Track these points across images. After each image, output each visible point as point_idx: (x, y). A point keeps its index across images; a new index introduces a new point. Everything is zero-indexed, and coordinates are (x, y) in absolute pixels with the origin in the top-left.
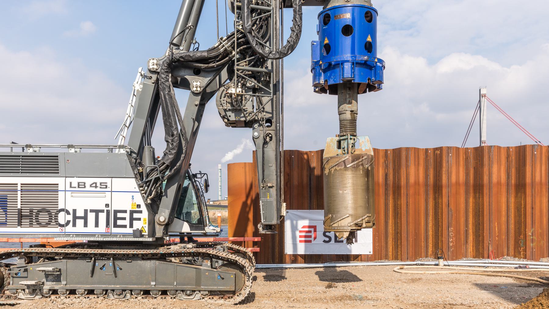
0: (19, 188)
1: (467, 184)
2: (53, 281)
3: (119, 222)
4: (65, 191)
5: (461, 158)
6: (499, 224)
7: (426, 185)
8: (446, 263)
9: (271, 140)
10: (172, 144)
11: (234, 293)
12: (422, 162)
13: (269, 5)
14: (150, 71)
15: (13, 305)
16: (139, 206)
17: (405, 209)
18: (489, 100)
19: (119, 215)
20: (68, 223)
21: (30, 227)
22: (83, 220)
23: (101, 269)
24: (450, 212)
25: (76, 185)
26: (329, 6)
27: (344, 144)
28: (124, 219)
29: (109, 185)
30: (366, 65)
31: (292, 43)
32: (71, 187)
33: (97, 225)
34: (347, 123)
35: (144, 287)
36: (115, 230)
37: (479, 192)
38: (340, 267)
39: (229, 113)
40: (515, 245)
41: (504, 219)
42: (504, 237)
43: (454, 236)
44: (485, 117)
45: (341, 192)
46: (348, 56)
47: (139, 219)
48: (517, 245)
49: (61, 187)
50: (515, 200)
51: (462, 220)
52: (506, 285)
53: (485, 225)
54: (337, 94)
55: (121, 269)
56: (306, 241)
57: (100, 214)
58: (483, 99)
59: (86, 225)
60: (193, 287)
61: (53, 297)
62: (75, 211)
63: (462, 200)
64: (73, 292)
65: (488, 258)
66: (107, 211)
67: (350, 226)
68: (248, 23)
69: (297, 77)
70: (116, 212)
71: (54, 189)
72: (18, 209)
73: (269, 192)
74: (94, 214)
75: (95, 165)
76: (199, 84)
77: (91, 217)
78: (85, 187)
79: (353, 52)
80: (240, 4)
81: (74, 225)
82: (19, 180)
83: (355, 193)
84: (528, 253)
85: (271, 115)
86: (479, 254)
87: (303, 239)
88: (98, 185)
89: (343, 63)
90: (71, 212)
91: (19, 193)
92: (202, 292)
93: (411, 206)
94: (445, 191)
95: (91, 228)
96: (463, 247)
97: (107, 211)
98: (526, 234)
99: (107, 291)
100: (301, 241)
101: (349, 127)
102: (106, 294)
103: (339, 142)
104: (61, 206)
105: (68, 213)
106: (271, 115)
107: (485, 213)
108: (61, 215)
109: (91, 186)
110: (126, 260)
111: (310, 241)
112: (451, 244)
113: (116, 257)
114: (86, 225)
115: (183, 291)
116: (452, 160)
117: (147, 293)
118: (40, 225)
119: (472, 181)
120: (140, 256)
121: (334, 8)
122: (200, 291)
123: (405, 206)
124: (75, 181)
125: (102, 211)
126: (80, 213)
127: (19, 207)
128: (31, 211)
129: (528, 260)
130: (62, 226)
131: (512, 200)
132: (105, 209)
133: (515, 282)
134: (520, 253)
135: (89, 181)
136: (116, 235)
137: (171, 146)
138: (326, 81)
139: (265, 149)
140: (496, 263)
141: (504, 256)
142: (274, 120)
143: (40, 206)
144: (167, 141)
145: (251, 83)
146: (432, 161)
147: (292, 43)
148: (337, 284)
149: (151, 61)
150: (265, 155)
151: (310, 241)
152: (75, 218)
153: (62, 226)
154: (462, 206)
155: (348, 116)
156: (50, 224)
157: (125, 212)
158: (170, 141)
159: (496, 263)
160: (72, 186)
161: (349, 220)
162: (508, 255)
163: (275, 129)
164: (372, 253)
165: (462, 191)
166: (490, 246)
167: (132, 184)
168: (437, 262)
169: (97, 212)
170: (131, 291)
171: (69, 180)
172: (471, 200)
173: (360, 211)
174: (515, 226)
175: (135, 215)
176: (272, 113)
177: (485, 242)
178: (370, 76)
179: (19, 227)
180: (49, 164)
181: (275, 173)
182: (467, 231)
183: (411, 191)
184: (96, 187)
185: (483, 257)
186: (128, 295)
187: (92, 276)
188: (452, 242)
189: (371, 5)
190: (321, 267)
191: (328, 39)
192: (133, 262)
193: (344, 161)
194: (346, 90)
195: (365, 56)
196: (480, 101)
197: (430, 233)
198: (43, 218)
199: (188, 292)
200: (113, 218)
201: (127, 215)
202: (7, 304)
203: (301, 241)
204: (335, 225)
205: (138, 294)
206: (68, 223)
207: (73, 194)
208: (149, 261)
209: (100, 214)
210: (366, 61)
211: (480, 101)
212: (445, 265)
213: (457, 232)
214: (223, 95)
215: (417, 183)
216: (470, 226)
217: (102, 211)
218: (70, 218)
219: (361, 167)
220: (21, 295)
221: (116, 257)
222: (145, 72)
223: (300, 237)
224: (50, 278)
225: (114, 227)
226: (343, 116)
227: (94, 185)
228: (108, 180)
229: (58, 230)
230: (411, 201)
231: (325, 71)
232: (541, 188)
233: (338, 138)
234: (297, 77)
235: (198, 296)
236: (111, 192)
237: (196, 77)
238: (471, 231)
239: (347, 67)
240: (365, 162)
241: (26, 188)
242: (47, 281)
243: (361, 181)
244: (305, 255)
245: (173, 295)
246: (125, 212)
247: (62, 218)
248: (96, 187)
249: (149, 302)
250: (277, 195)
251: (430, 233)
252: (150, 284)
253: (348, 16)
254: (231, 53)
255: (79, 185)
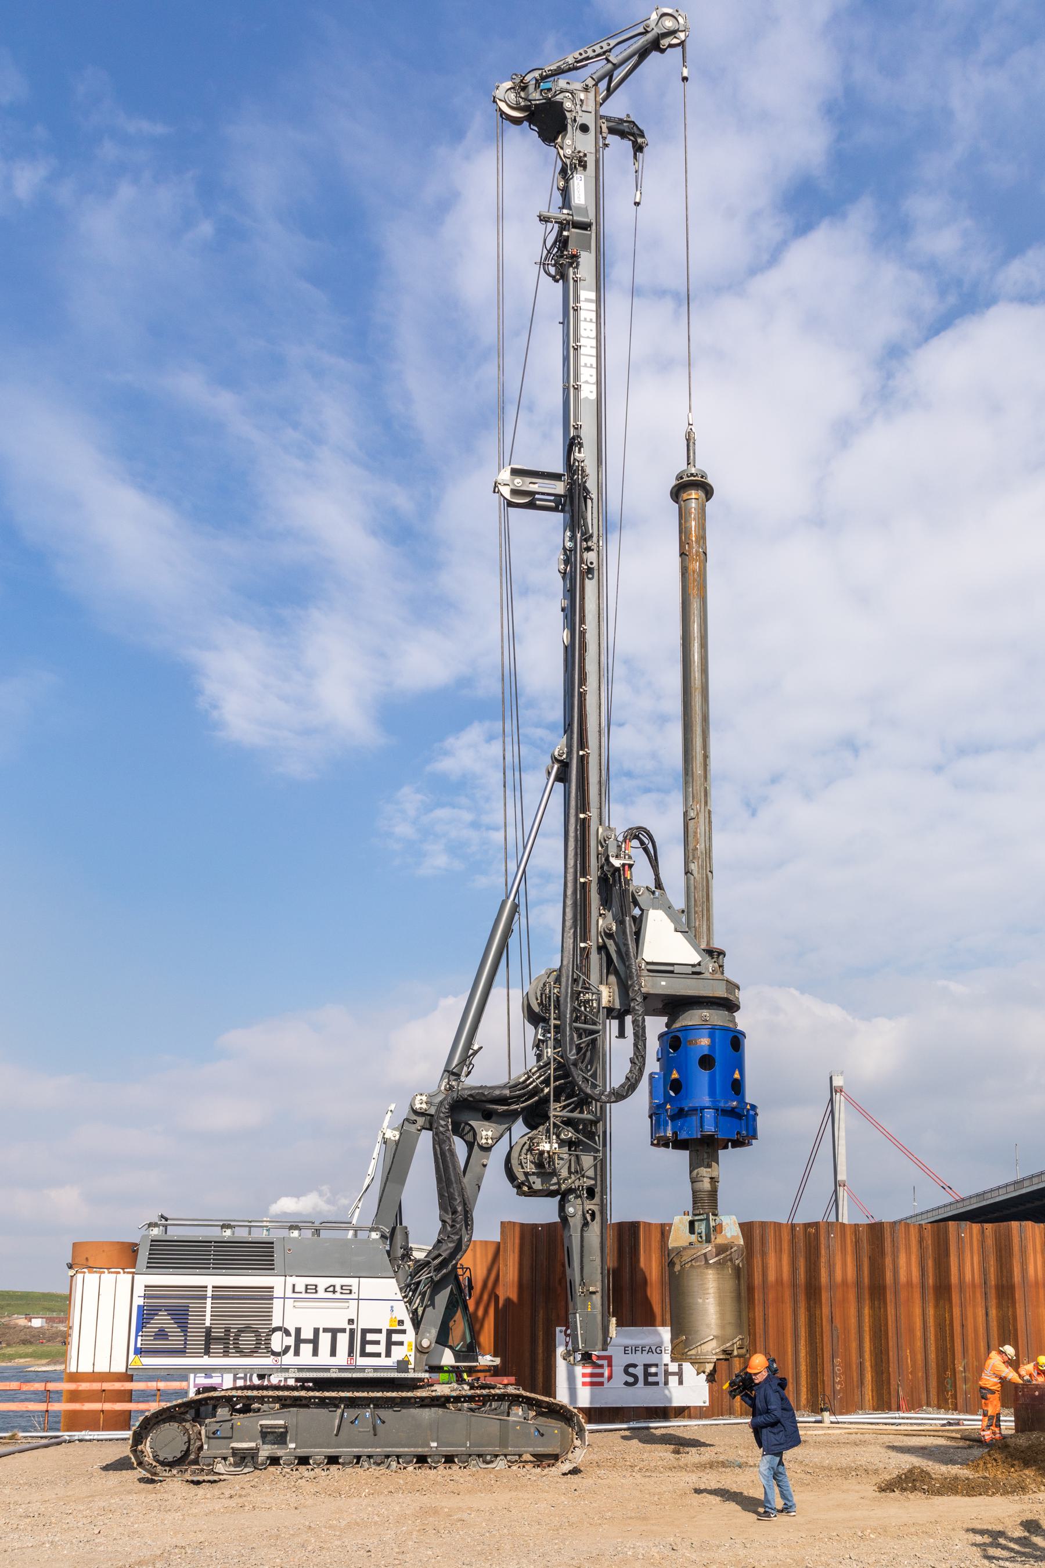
0: (209, 1293)
1: (858, 1284)
2: (274, 1444)
3: (369, 1349)
4: (284, 1298)
5: (849, 1241)
6: (913, 1353)
7: (794, 1285)
8: (833, 1418)
9: (593, 1219)
10: (452, 1226)
11: (556, 1457)
12: (786, 1246)
13: (594, 1023)
14: (415, 1112)
15: (215, 1481)
16: (401, 1322)
17: (762, 1326)
18: (849, 1100)
19: (370, 1337)
20: (287, 1349)
21: (224, 1356)
22: (311, 1345)
23: (352, 1422)
24: (835, 1333)
25: (303, 1290)
26: (677, 1025)
27: (700, 1227)
28: (378, 1343)
29: (355, 1289)
30: (733, 1113)
31: (633, 1081)
32: (294, 1292)
33: (333, 1353)
34: (703, 1195)
35: (420, 1450)
36: (362, 1361)
37: (879, 1299)
38: (656, 1428)
39: (532, 1179)
40: (938, 1387)
41: (919, 1344)
42: (920, 1374)
43: (842, 1374)
44: (843, 1134)
45: (700, 1301)
46: (706, 1100)
47: (401, 1343)
48: (941, 1389)
49: (278, 1292)
50: (935, 1312)
51: (854, 1345)
52: (938, 1447)
53: (891, 1354)
54: (687, 1149)
55: (384, 1422)
56: (592, 1384)
57: (339, 1335)
58: (837, 1097)
59: (315, 1353)
60: (497, 1450)
61: (271, 1469)
62: (298, 1331)
63: (853, 1311)
64: (304, 1461)
65: (899, 1409)
66: (351, 1330)
67: (716, 1354)
68: (571, 1050)
69: (629, 1121)
70: (365, 1332)
71: (266, 1295)
72: (206, 1328)
73: (591, 1300)
74: (329, 1335)
75: (327, 1254)
76: (490, 1133)
77: (325, 1339)
78: (316, 1292)
79: (712, 1093)
80: (558, 1022)
81: (297, 1353)
82: (210, 1281)
83: (721, 1303)
84: (960, 1401)
85: (593, 1182)
86: (883, 1403)
87: (588, 1380)
88: (338, 1288)
89: (702, 1109)
90: (293, 1333)
91: (209, 1301)
92: (509, 1458)
93: (771, 1322)
94: (825, 1296)
95: (324, 1358)
96: (857, 1392)
97: (351, 1330)
98: (954, 1369)
99: (358, 1458)
100: (584, 1384)
101: (705, 1203)
102: (358, 1463)
103: (692, 1224)
104: (276, 1322)
105: (287, 1333)
106: (593, 1182)
107: (890, 1334)
108: (277, 1337)
109: (326, 1291)
110: (392, 1407)
111: (601, 1384)
112: (838, 1387)
113: (378, 1403)
114: (315, 1353)
115: (479, 1456)
116: (836, 1245)
117: (422, 1459)
118: (241, 1353)
119: (866, 1280)
120: (413, 1401)
121: (686, 1029)
122: (505, 1456)
123: (762, 1321)
124: (301, 1283)
125: (343, 1331)
126: (307, 1334)
127: (208, 1324)
128: (227, 1331)
129: (960, 1412)
130: (274, 1354)
131: (931, 1311)
132: (348, 1327)
133: (949, 1443)
134: (946, 1400)
135: (323, 1283)
136: (362, 1369)
137: (449, 1229)
138: (675, 1133)
139: (585, 1234)
140: (911, 1418)
141: (922, 1406)
142: (598, 1190)
143: (242, 1323)
144: (443, 1221)
145: (568, 1134)
146: (801, 1245)
147: (633, 1081)
148: (687, 1449)
149: (419, 1097)
150: (585, 1244)
151: (601, 1384)
152: (299, 1341)
153: (274, 1354)
154: (853, 1321)
155: (706, 1185)
156: (256, 1352)
157: (379, 1331)
158: (449, 1221)
159: (911, 1418)
160: (296, 1290)
161: (713, 1344)
162: (928, 1405)
163: (599, 1202)
164: (707, 1404)
165: (852, 1296)
166: (900, 1389)
167: (390, 1287)
168: (819, 1418)
169: (334, 1332)
170: (398, 1457)
171: (291, 1280)
172: (866, 1311)
173: (730, 1330)
174: (937, 1356)
175: (395, 1337)
176: (595, 1179)
177: (893, 1382)
178: (739, 1125)
179: (206, 1357)
180: (259, 1255)
181: (599, 1271)
182: (861, 1364)
183: (771, 1296)
184: (334, 1292)
185: (890, 1409)
186: (394, 1464)
187: (106, 1468)
188: (839, 1382)
189: (736, 1024)
190: (625, 1430)
191: (678, 1072)
192: (404, 1411)
193: (705, 1255)
194: (704, 1149)
195: (733, 1101)
196: (831, 1100)
197: (803, 1368)
198: (247, 1340)
199: (488, 1458)
200: (360, 1340)
201: (382, 1337)
202: (204, 1481)
203: (584, 1384)
204: (693, 1352)
205: (409, 1463)
206: (287, 1349)
207: (296, 1304)
208: (427, 1410)
209: (339, 1335)
210: (733, 1109)
211: (831, 1100)
212: (832, 1423)
213: (847, 1366)
214: (524, 1151)
215: (779, 1282)
216: (867, 1356)
217: (343, 1331)
218: (290, 1341)
219: (729, 1263)
220: (220, 1468)
221: (378, 1403)
222: (405, 1113)
223: (584, 1375)
224: (270, 1438)
225: (361, 1356)
226: (698, 1185)
227: (331, 1289)
228: (353, 1282)
229: (269, 1361)
230: (771, 1312)
231: (673, 1118)
232: (974, 1293)
233: (690, 1218)
234: (629, 1121)
235: (501, 1464)
236: (358, 1299)
237: (486, 1123)
238: (868, 1364)
239: (709, 1114)
240: (735, 1256)
241: (221, 1294)
242: (264, 1443)
243: (730, 1284)
244: (590, 1409)
245: (464, 1462)
246: (379, 1331)
247: (277, 1342)
248: (334, 1292)
249: (425, 1472)
250: (602, 1305)
251: (803, 1368)
252: (428, 1446)
253: (705, 1041)
254: (542, 1090)
255: (307, 1289)
